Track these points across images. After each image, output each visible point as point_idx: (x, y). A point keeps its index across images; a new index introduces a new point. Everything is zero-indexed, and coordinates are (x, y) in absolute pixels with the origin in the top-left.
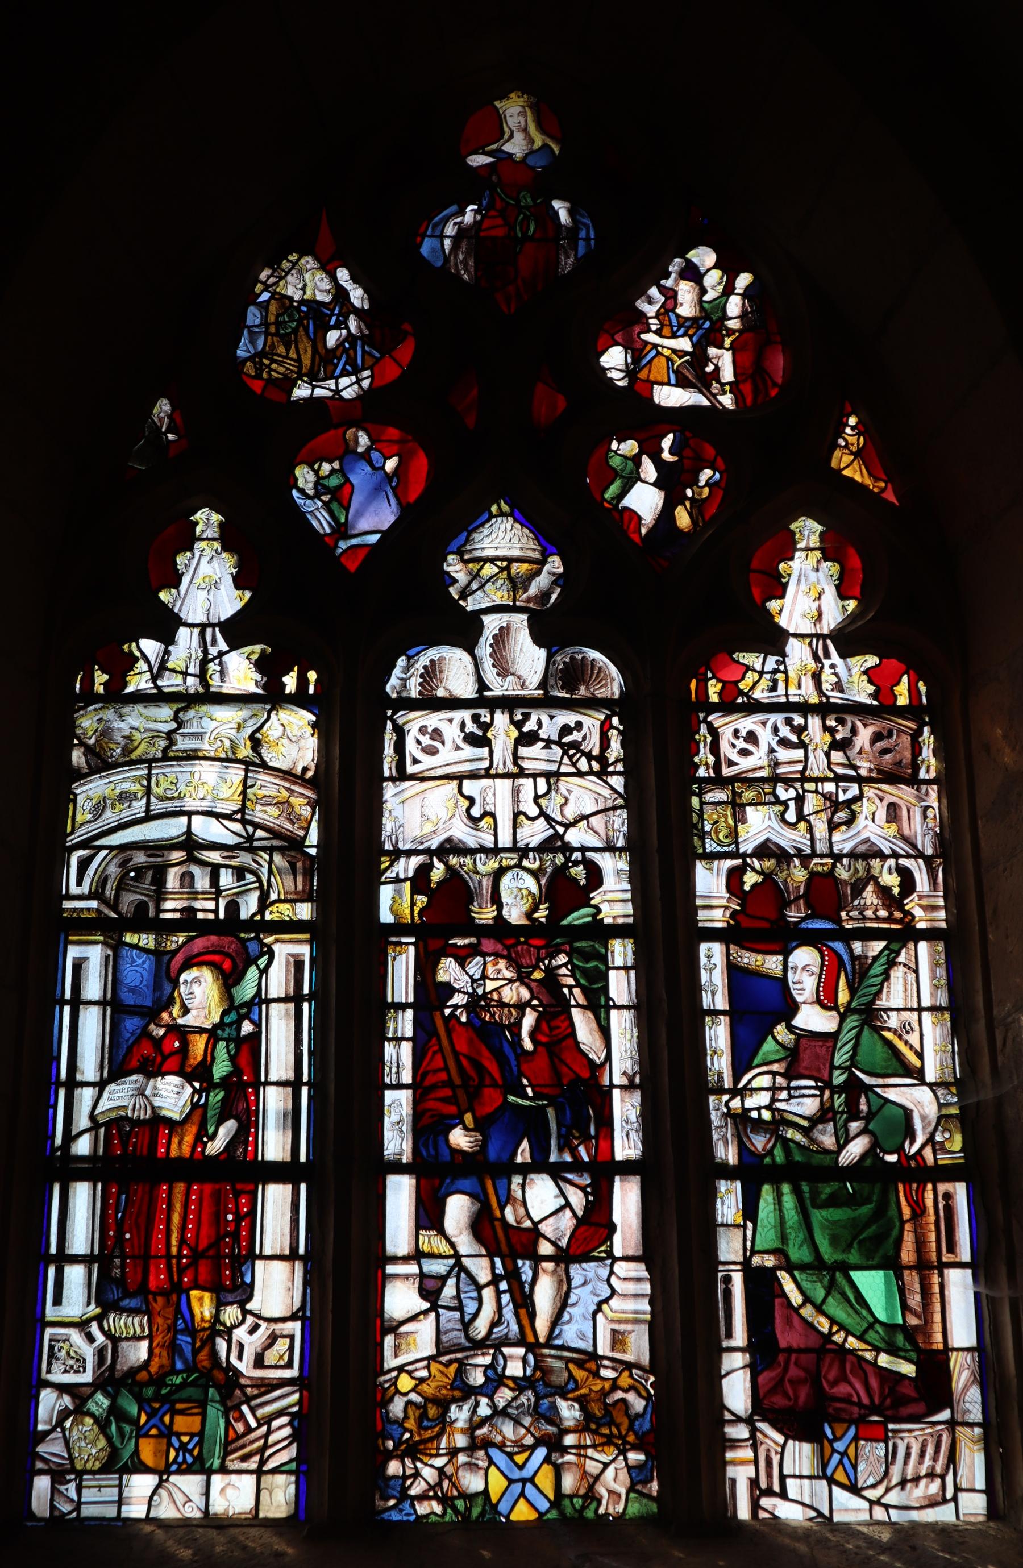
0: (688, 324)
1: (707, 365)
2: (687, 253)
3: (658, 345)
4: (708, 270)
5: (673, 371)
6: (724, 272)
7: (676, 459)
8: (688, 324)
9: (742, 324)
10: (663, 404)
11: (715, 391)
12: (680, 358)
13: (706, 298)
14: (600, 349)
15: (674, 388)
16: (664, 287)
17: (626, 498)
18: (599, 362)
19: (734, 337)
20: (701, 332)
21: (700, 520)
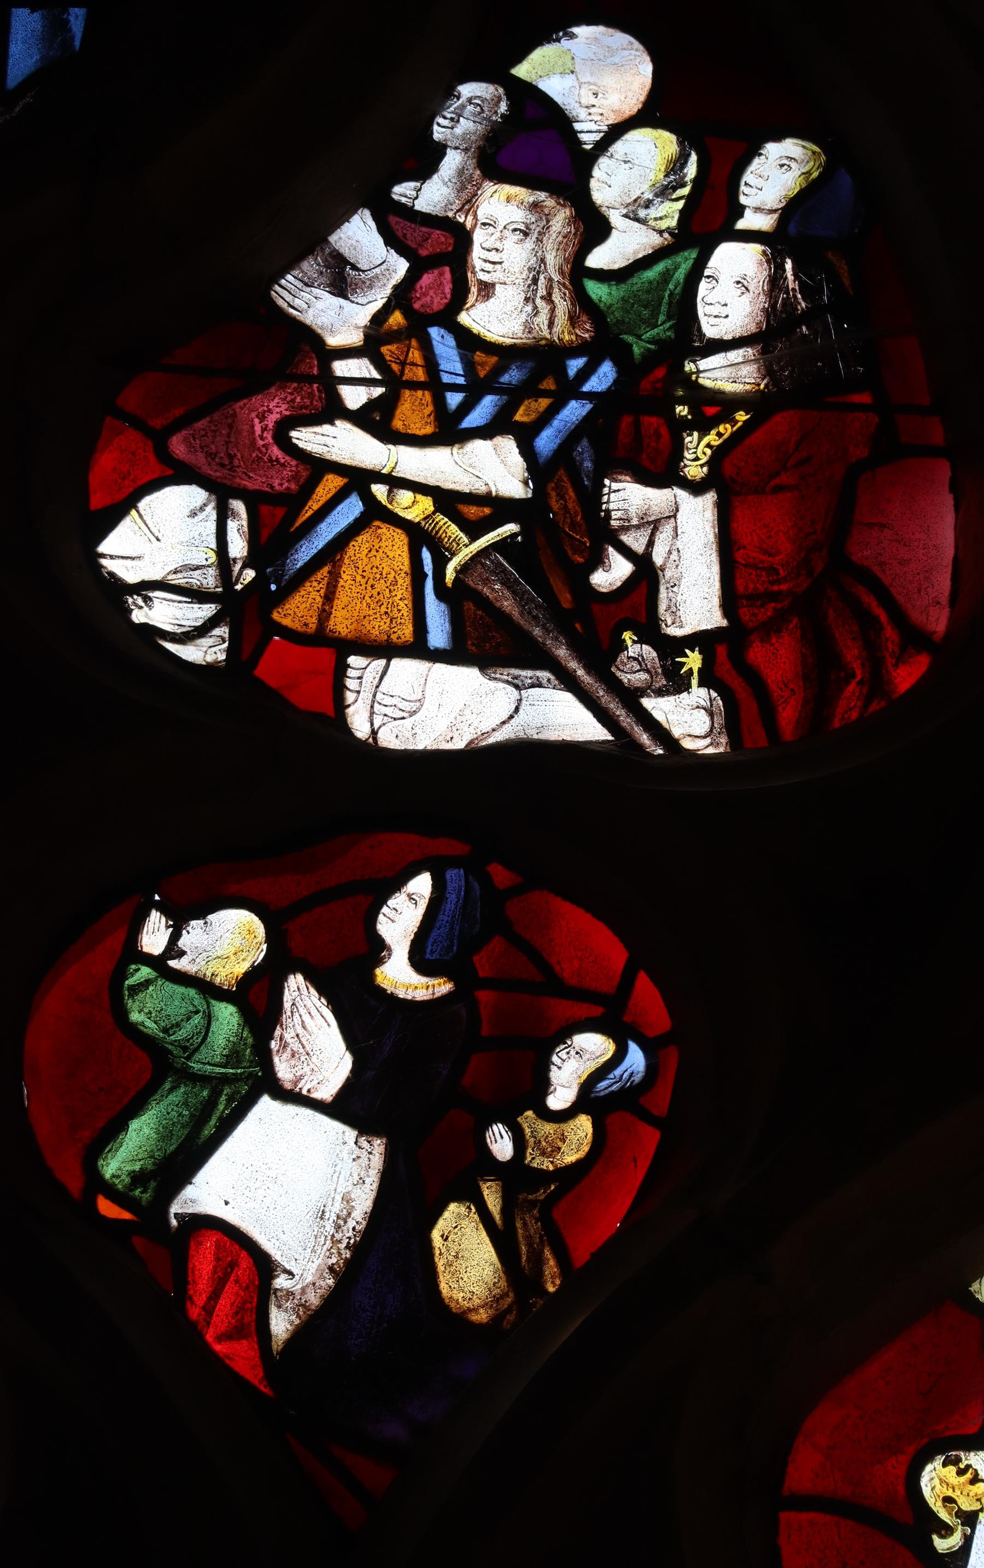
0: (512, 376)
1: (597, 561)
2: (520, 57)
3: (376, 476)
4: (616, 132)
5: (442, 592)
6: (687, 139)
7: (443, 987)
8: (512, 376)
9: (768, 371)
10: (389, 739)
11: (632, 677)
12: (474, 530)
13: (598, 258)
14: (97, 501)
15: (441, 670)
16: (408, 213)
17: (202, 1176)
18: (94, 558)
19: (726, 429)
20: (574, 411)
21: (551, 1266)
